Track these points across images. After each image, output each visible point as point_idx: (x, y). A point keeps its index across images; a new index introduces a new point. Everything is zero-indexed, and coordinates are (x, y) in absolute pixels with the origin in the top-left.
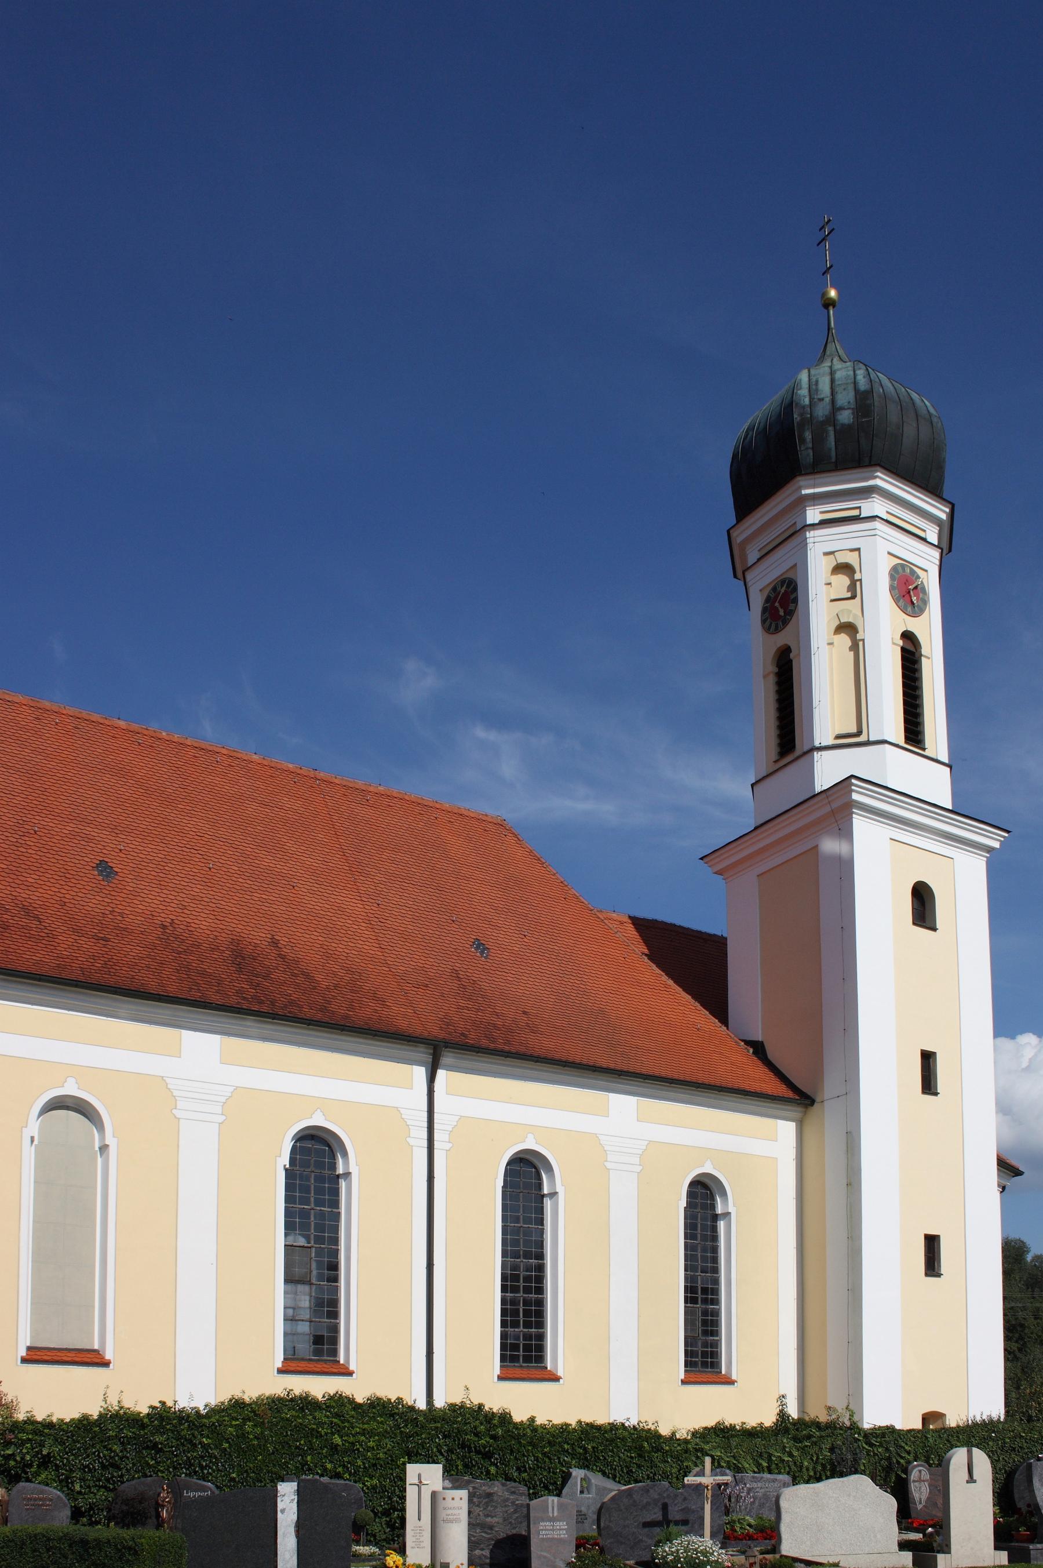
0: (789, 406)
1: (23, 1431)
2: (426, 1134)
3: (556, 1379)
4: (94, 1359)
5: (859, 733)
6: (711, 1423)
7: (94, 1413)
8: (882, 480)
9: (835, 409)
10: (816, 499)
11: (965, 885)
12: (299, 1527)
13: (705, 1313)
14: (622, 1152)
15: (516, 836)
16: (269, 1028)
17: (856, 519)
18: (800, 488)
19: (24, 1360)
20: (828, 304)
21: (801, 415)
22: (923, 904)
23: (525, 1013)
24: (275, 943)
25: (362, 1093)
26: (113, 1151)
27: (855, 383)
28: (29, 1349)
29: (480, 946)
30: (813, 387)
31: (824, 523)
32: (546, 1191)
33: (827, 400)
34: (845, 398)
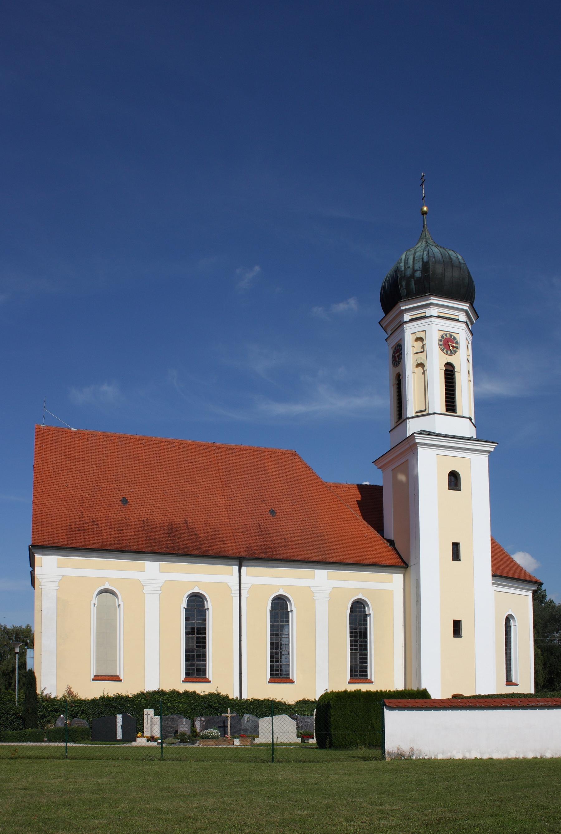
0: (397, 270)
1: (76, 703)
2: (237, 592)
3: (293, 682)
4: (116, 679)
5: (425, 411)
6: (301, 699)
7: (98, 697)
8: (434, 300)
9: (414, 271)
10: (408, 310)
11: (477, 469)
12: (122, 726)
13: (361, 655)
14: (320, 593)
15: (300, 458)
16: (174, 558)
17: (424, 317)
18: (400, 307)
19: (93, 680)
20: (424, 213)
21: (400, 275)
22: (454, 481)
23: (285, 539)
24: (186, 522)
25: (212, 579)
26: (122, 607)
27: (423, 258)
28: (95, 676)
29: (272, 512)
30: (407, 260)
31: (412, 320)
32: (289, 610)
33: (411, 267)
34: (419, 265)
